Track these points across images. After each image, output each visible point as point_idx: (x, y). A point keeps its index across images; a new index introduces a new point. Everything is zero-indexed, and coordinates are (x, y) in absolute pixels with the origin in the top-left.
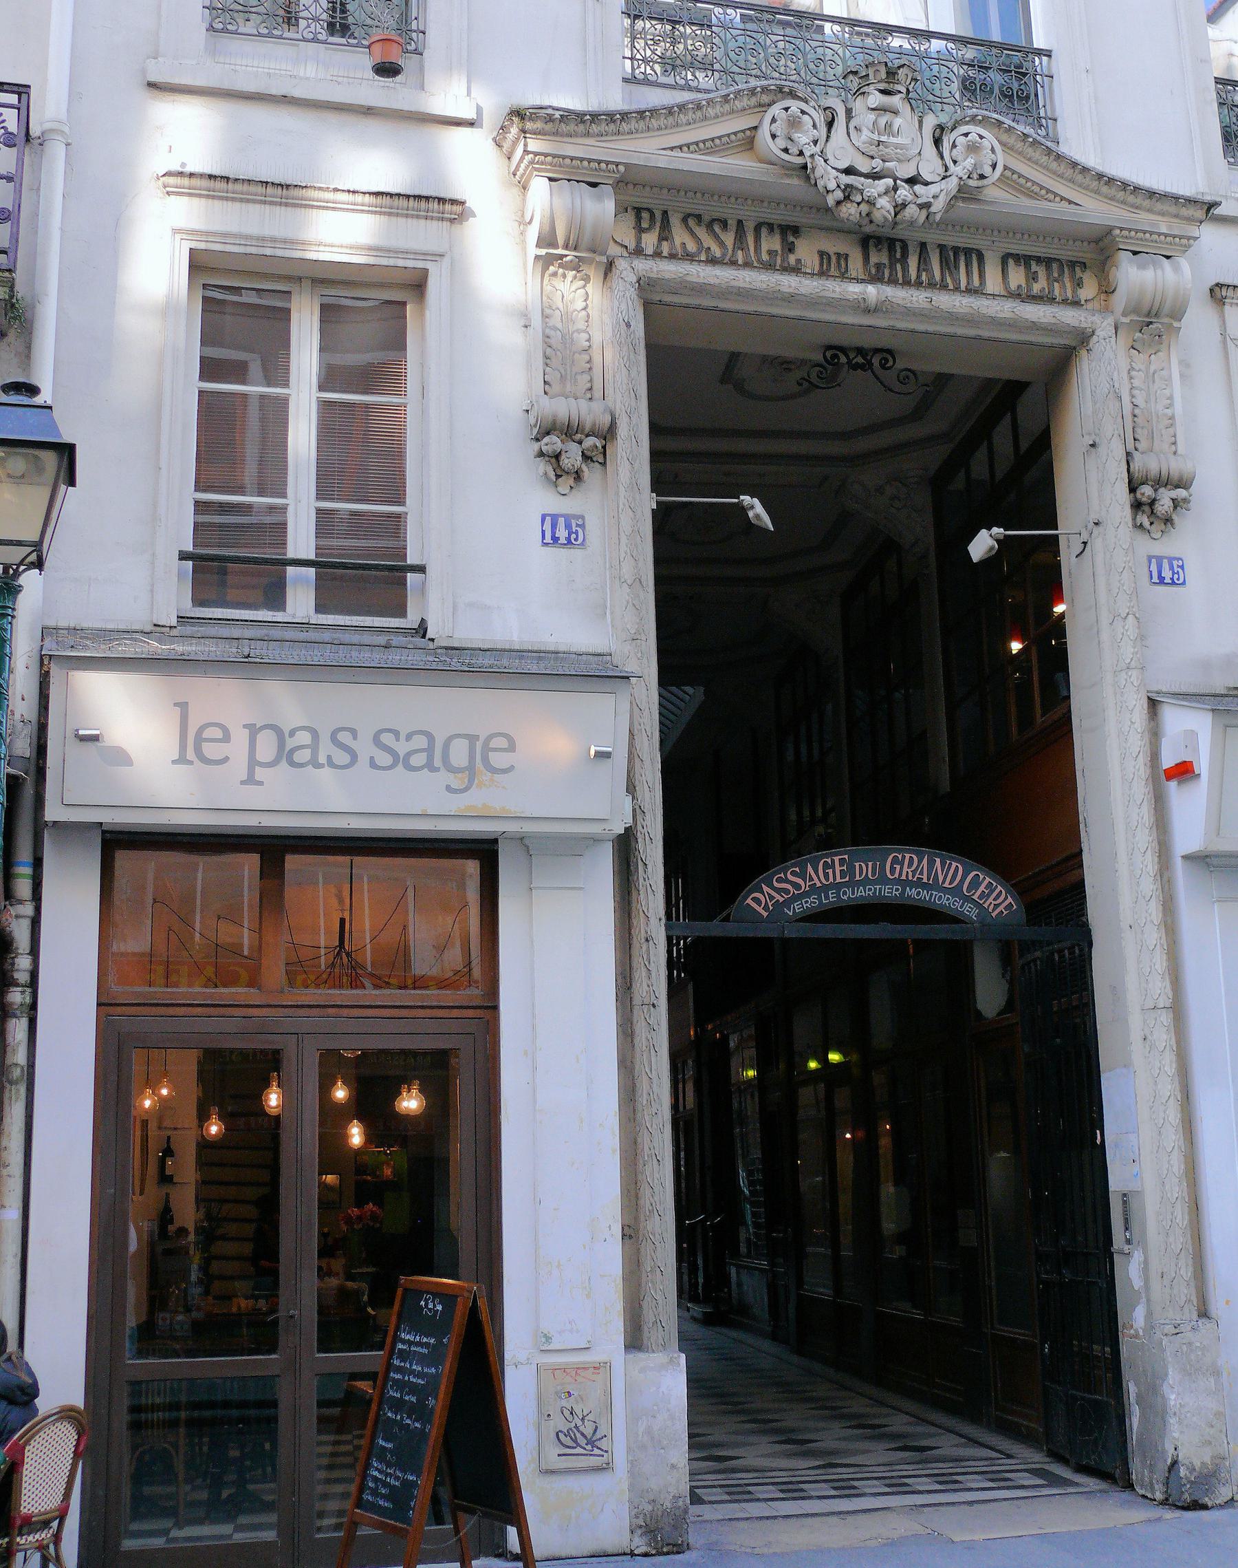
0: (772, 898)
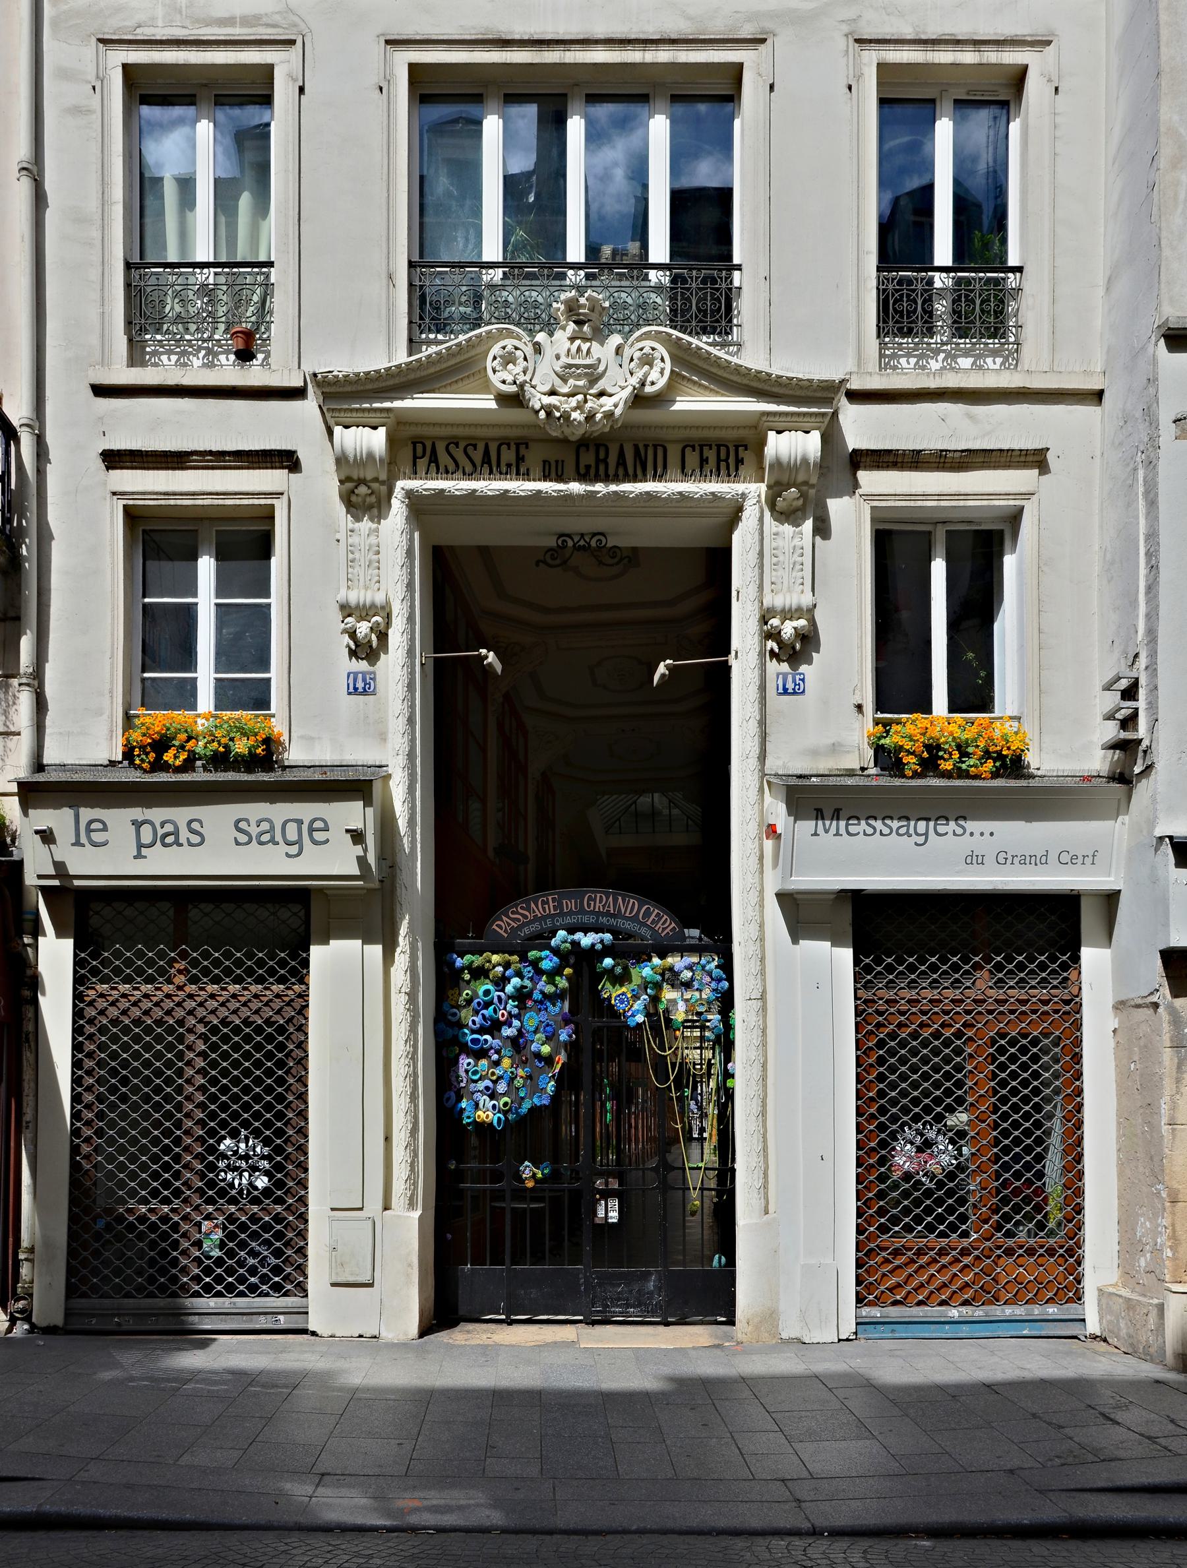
0: (509, 924)
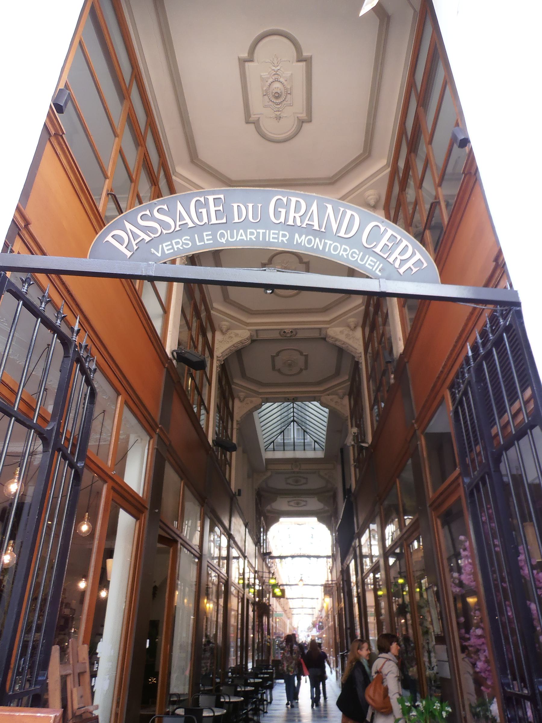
0: (135, 236)
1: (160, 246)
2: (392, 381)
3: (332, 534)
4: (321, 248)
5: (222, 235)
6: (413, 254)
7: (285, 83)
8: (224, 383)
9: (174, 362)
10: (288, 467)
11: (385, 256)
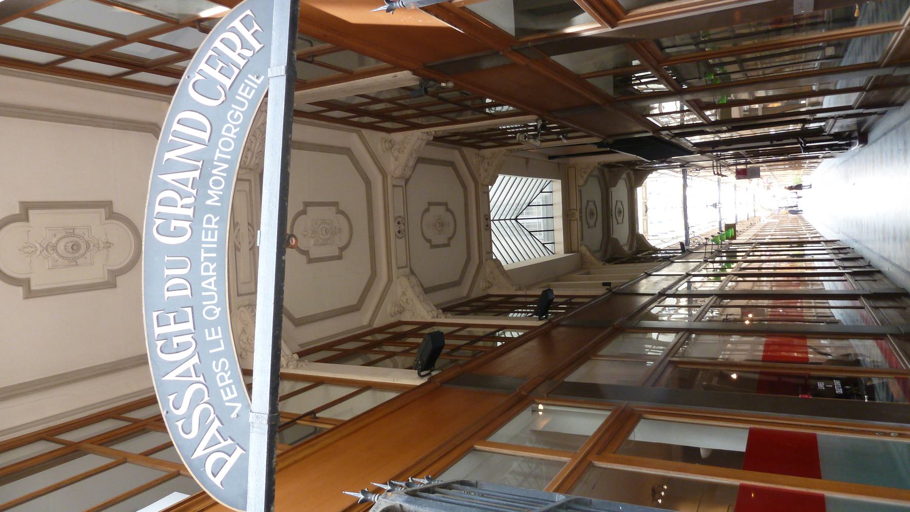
0: (213, 442)
1: (227, 404)
2: (451, 84)
3: (656, 169)
4: (226, 166)
5: (210, 313)
6: (234, 30)
7: (59, 236)
8: (467, 308)
9: (434, 373)
10: (575, 225)
11: (237, 71)
